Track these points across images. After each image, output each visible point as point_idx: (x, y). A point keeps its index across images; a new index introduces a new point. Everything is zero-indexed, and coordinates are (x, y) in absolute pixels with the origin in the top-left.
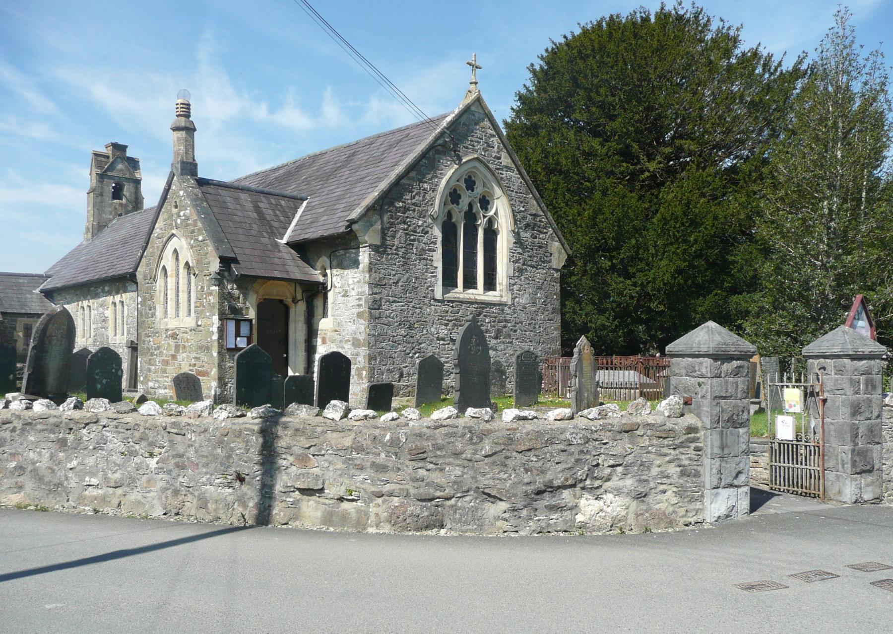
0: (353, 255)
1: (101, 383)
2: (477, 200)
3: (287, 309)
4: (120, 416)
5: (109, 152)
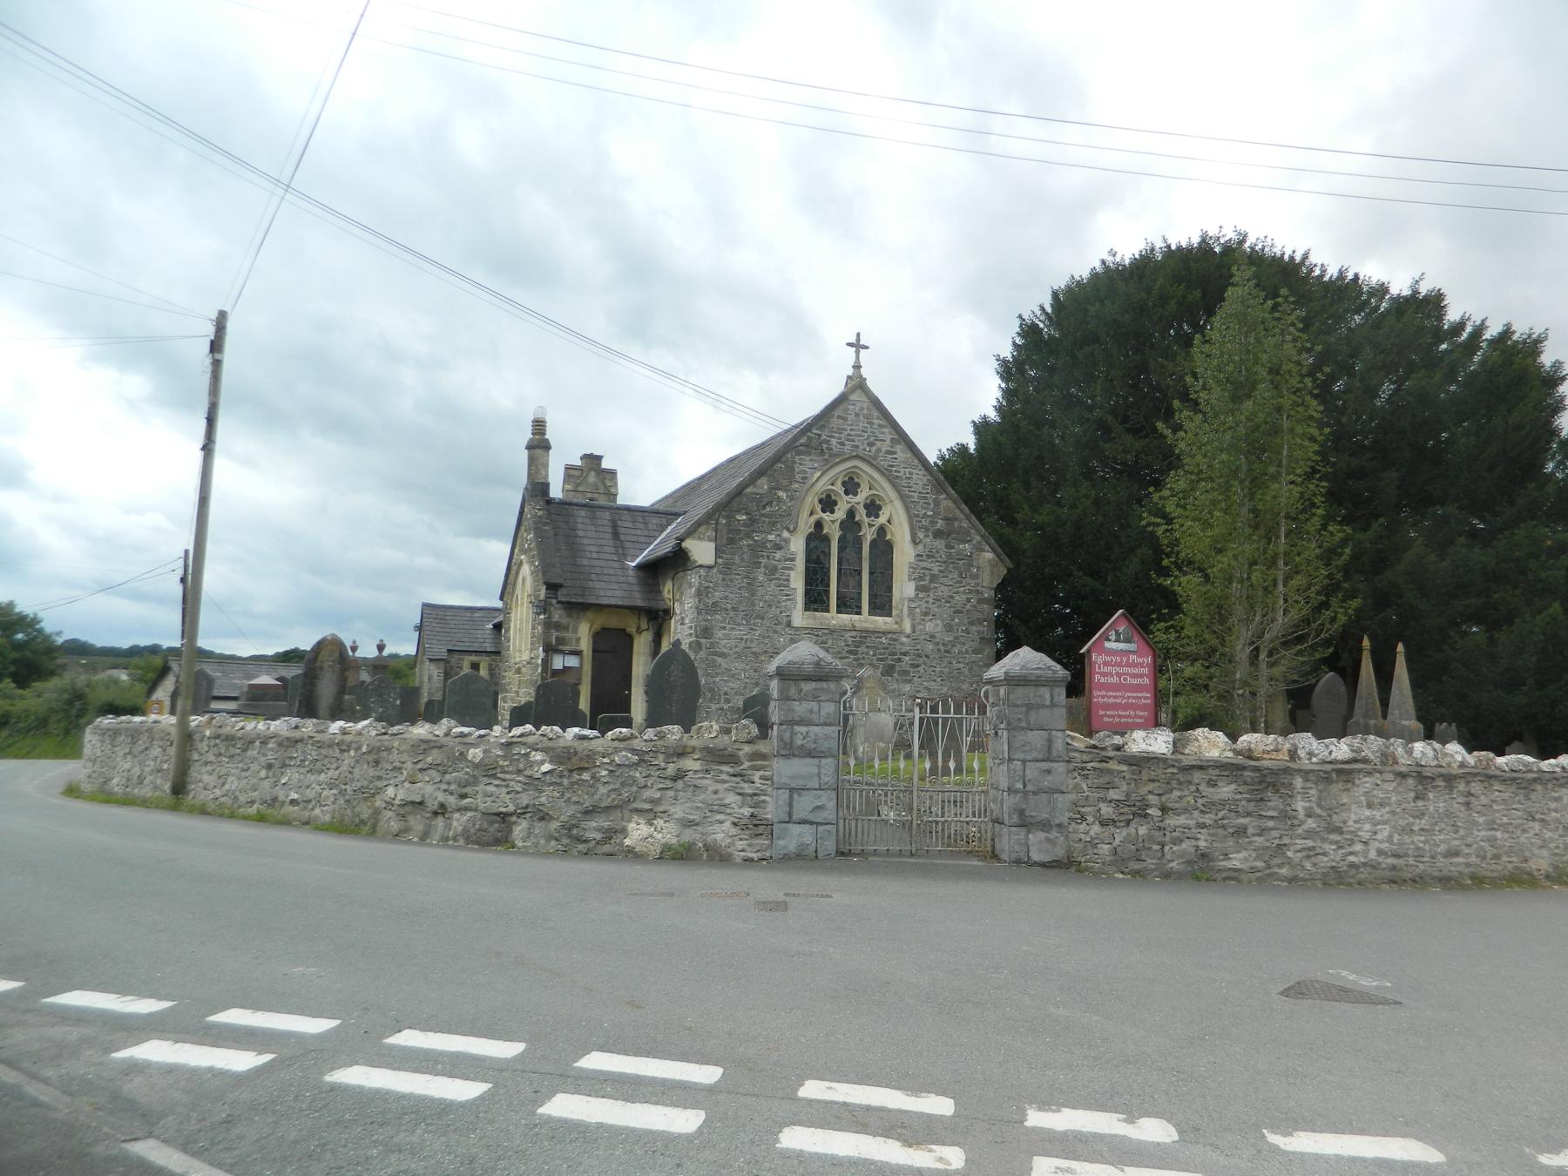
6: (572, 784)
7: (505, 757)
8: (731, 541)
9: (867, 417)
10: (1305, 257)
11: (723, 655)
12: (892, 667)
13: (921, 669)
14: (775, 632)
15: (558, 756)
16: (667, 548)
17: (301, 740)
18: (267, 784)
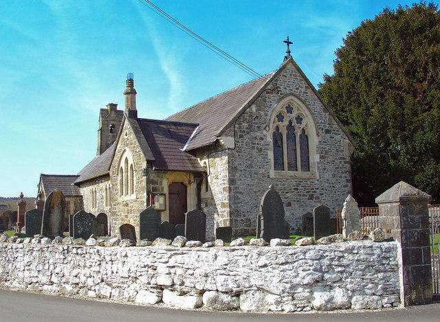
3: (186, 187)
5: (108, 108)
11: (241, 193)
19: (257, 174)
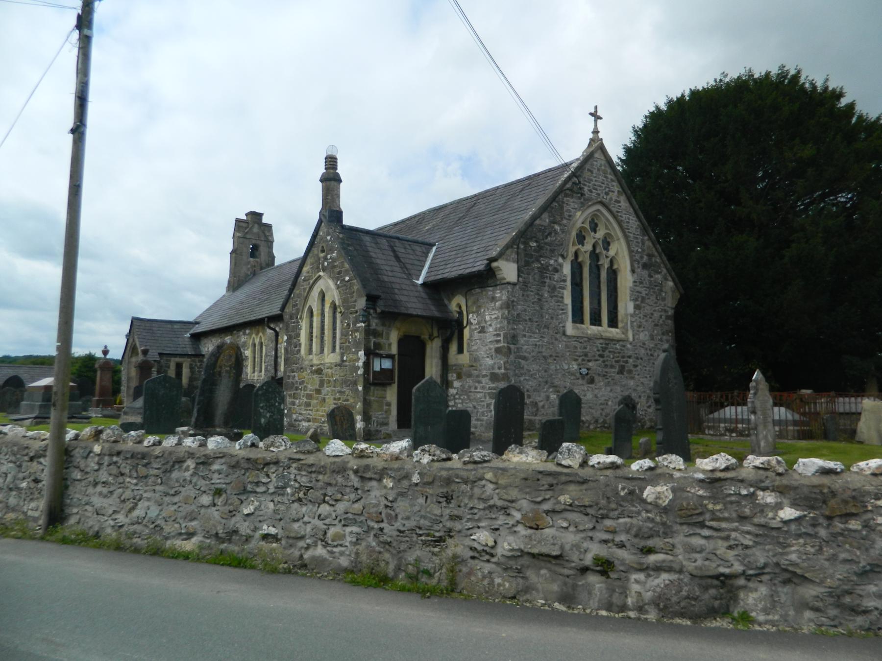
0: (490, 293)
1: (265, 417)
2: (600, 242)
4: (302, 457)
6: (835, 535)
7: (714, 498)
8: (527, 264)
9: (605, 172)
10: (841, 88)
11: (525, 358)
12: (623, 367)
13: (638, 368)
14: (556, 339)
15: (806, 498)
16: (480, 266)
17: (277, 463)
18: (215, 514)
19: (548, 328)
